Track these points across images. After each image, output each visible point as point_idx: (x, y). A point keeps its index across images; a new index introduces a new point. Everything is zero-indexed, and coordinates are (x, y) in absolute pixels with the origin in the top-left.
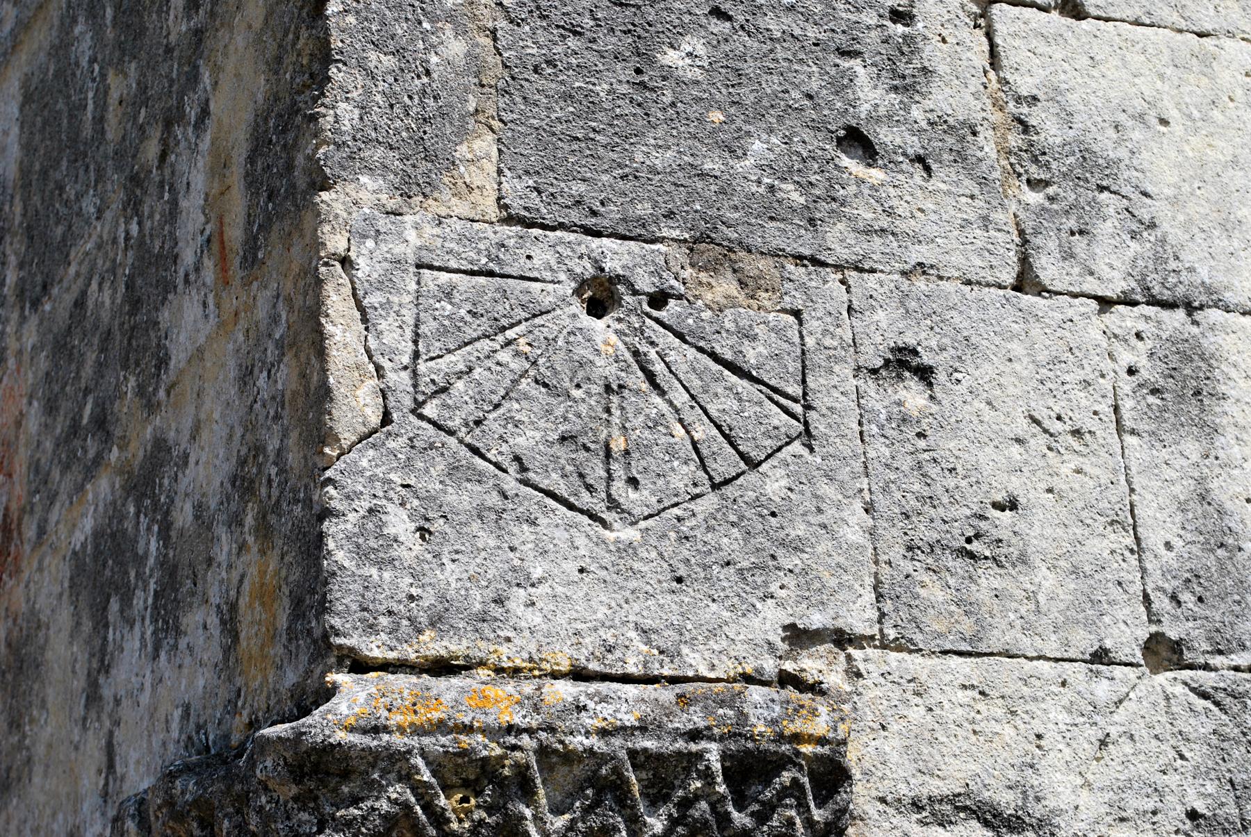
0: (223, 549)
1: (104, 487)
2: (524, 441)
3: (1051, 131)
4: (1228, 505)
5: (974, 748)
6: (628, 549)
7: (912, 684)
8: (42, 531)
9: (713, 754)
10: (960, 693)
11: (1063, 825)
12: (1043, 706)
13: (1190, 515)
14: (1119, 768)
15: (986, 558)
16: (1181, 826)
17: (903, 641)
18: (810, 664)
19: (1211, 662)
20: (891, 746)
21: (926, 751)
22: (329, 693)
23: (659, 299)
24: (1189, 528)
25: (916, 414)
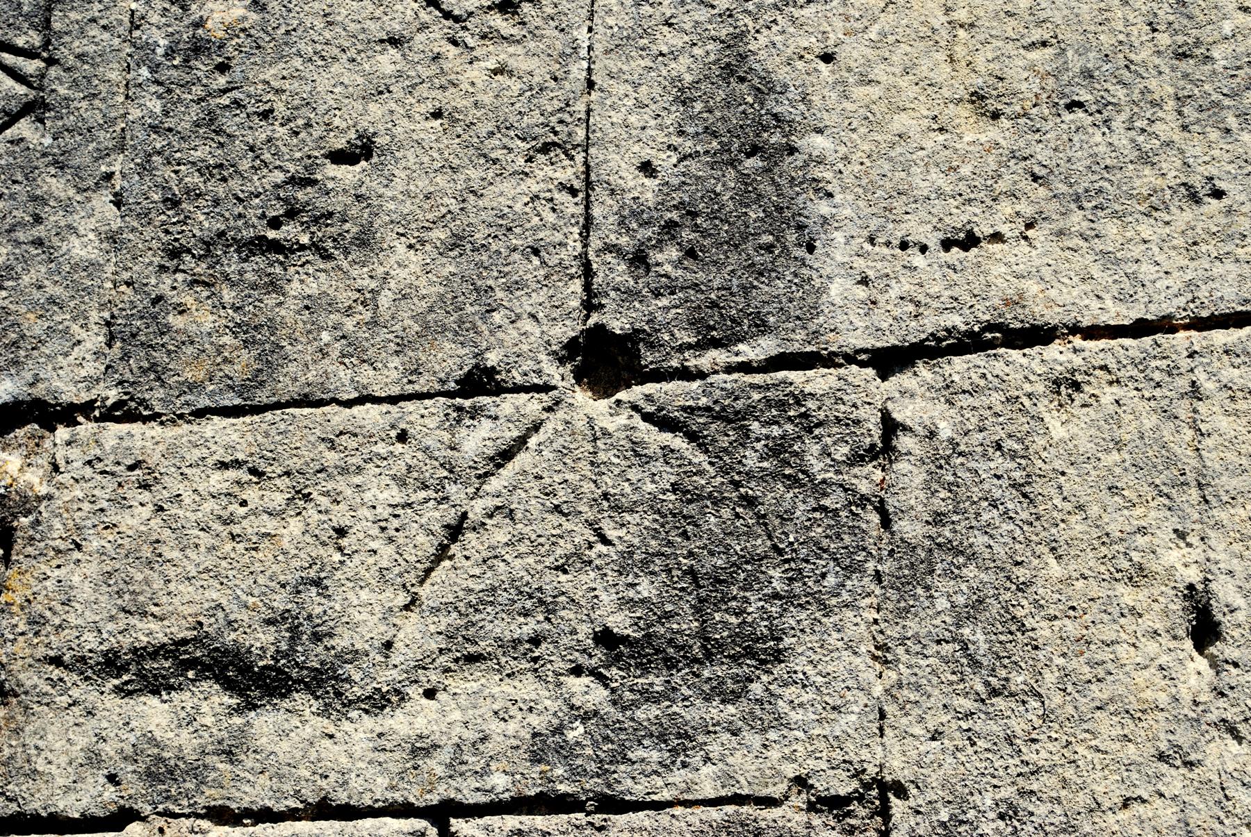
4: (782, 74)
5: (224, 564)
7: (137, 472)
10: (217, 476)
11: (357, 677)
12: (357, 480)
13: (699, 106)
14: (477, 571)
15: (303, 248)
16: (582, 660)
17: (133, 404)
19: (692, 363)
21: (139, 577)
24: (691, 130)
25: (220, 34)
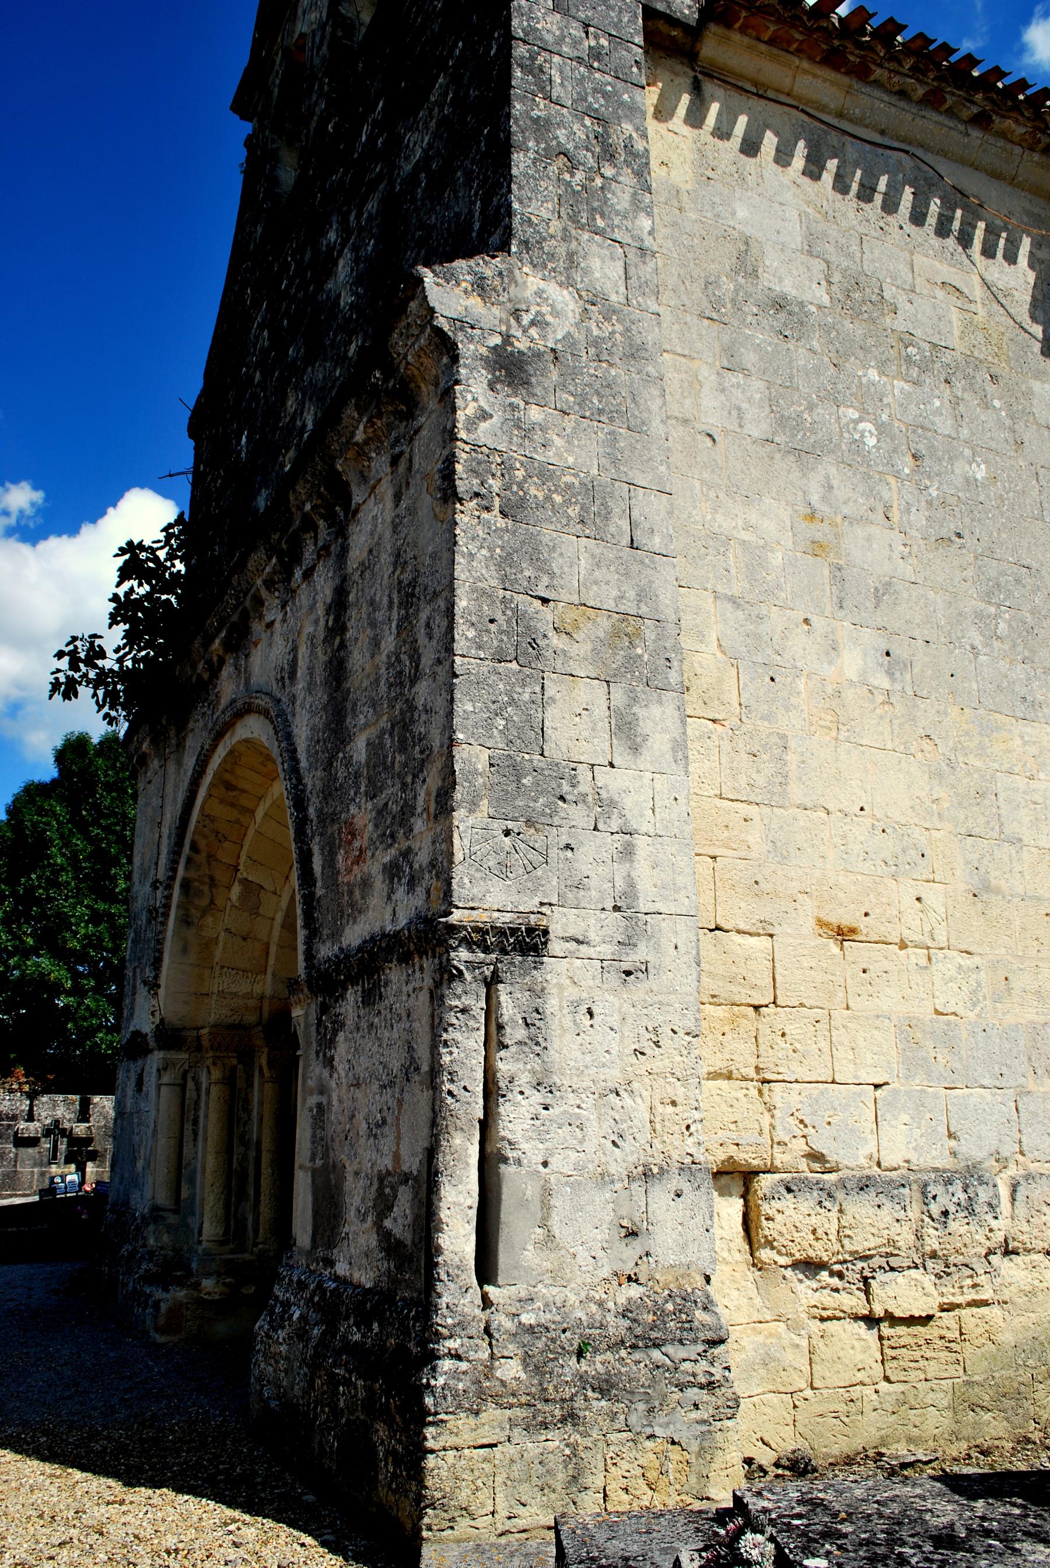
0: (427, 876)
1: (393, 852)
2: (491, 864)
3: (604, 795)
6: (509, 886)
8: (373, 855)
9: (523, 928)
18: (544, 909)
20: (558, 926)
22: (452, 913)
23: (518, 834)
